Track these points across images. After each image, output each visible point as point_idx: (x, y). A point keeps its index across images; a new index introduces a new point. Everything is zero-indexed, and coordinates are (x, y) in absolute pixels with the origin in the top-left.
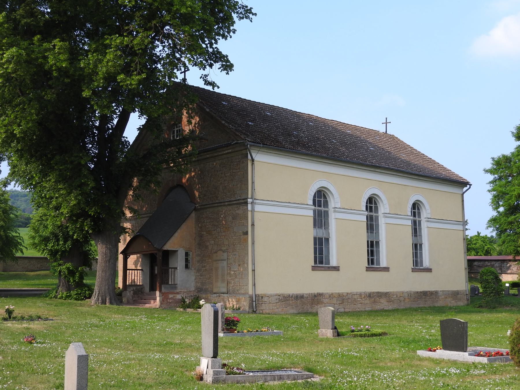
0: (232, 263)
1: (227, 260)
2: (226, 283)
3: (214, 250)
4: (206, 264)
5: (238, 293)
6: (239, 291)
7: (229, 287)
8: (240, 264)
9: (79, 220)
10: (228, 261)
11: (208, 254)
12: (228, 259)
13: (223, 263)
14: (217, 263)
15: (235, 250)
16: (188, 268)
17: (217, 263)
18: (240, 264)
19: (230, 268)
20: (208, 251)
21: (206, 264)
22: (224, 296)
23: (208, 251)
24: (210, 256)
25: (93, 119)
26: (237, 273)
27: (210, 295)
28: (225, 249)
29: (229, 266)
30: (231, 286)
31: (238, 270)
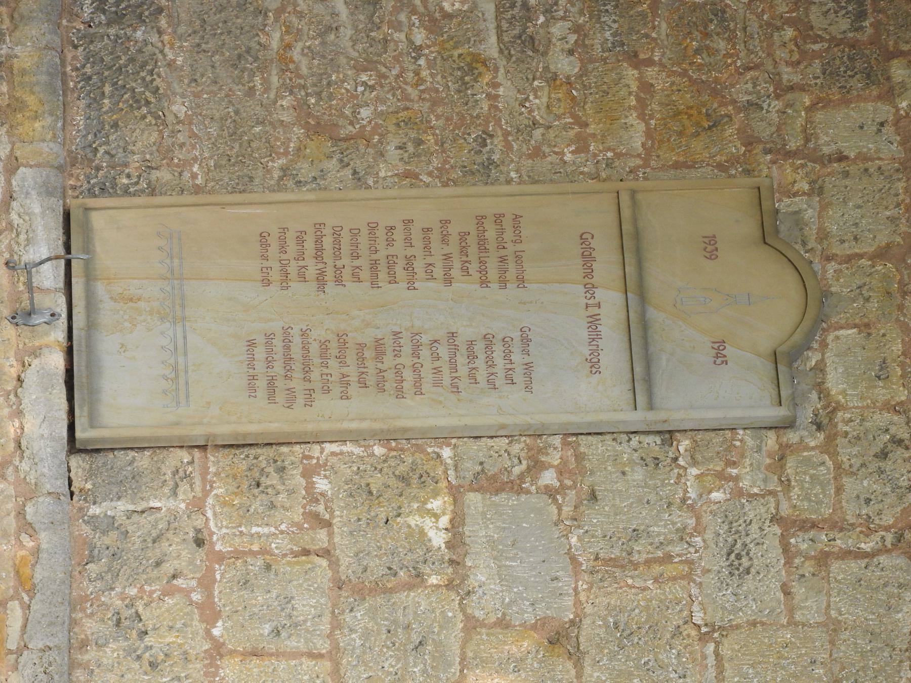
0: (594, 518)
1: (637, 418)
2: (252, 429)
3: (817, 190)
4: (566, 66)
5: (90, 627)
6: (112, 652)
7: (181, 476)
8: (577, 657)
9: (662, 555)
10: (626, 450)
11: (742, 92)
12: (669, 436)
13: (594, 366)
14: (588, 257)
15: (823, 559)
16: (631, 190)
17: (588, 257)
18: (577, 657)
19: (516, 487)
20: (783, 90)
21: (566, 66)
22: (31, 394)
23: (783, 90)
24: (716, 124)
25: (421, 679)
26: (419, 600)
27: (50, 149)
28: (835, 382)
29: (536, 466)
30: (198, 506)
31: (472, 625)
